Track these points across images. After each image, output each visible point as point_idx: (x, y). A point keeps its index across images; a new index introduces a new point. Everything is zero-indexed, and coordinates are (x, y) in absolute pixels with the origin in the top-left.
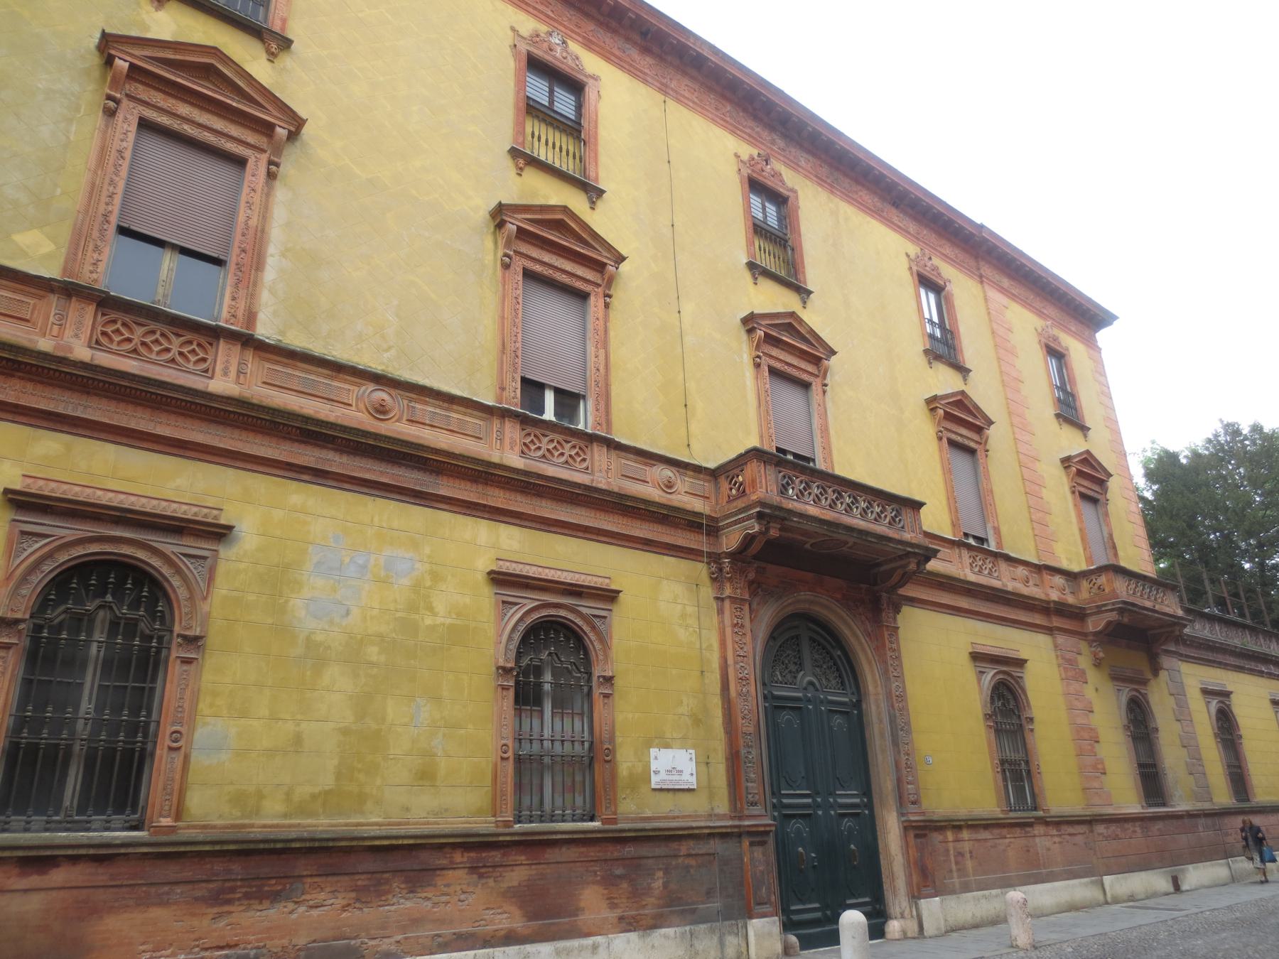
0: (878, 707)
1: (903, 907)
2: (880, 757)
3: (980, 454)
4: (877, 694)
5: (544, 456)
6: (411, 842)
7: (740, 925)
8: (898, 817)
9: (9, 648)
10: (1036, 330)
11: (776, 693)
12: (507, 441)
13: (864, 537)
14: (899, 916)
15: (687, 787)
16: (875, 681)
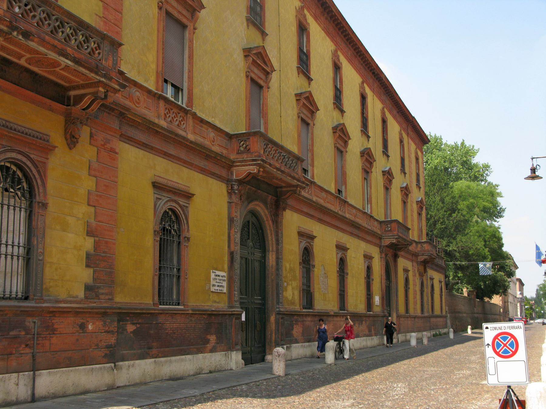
0: (394, 285)
3: (344, 153)
10: (296, 8)
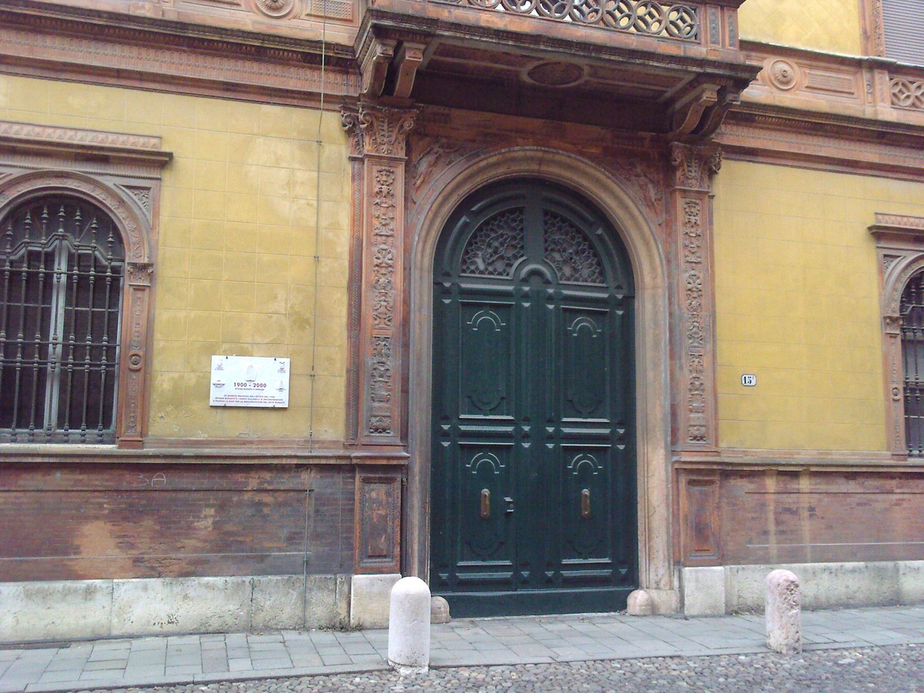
1: (660, 576)
2: (650, 375)
4: (655, 287)
5: (913, 105)
6: (385, 462)
7: (339, 580)
8: (666, 455)
9: (143, 290)
11: (464, 286)
12: (878, 94)
13: (593, 54)
14: (655, 586)
15: (271, 405)
16: (654, 269)
